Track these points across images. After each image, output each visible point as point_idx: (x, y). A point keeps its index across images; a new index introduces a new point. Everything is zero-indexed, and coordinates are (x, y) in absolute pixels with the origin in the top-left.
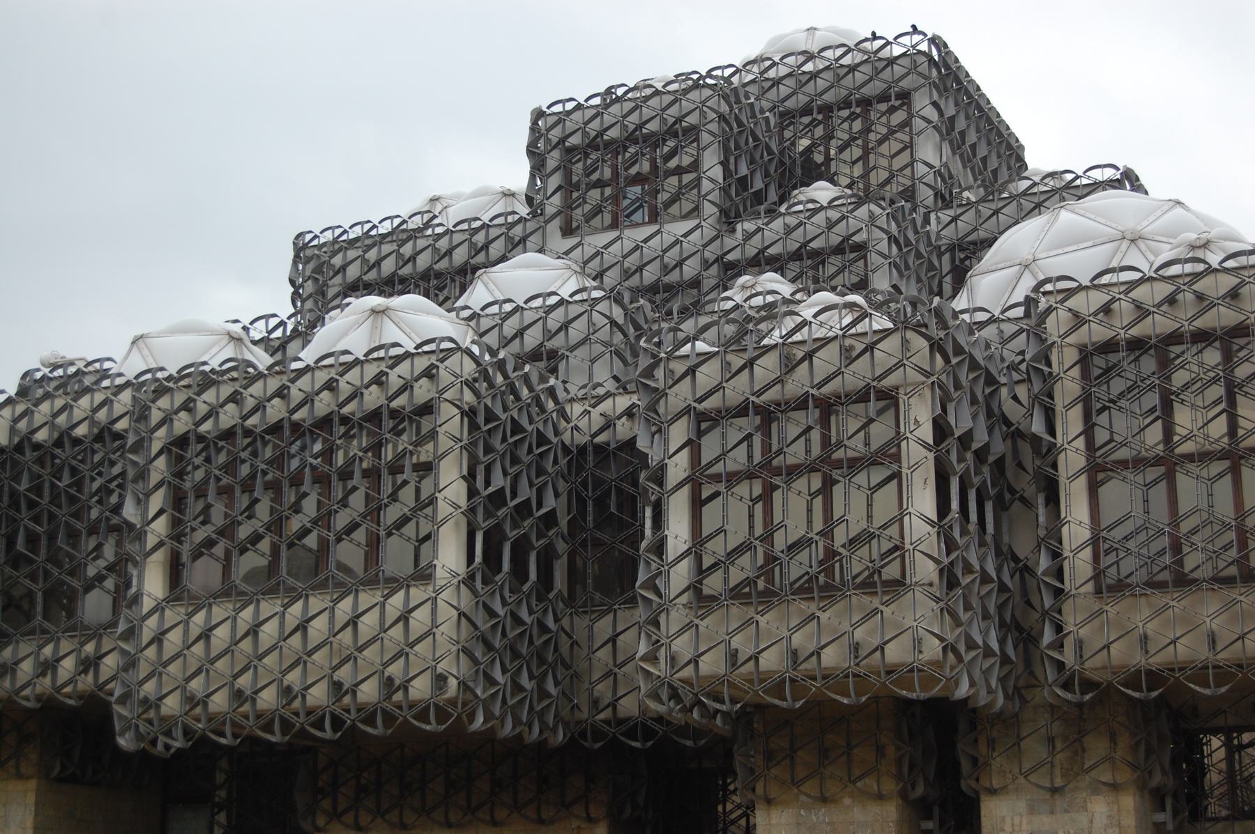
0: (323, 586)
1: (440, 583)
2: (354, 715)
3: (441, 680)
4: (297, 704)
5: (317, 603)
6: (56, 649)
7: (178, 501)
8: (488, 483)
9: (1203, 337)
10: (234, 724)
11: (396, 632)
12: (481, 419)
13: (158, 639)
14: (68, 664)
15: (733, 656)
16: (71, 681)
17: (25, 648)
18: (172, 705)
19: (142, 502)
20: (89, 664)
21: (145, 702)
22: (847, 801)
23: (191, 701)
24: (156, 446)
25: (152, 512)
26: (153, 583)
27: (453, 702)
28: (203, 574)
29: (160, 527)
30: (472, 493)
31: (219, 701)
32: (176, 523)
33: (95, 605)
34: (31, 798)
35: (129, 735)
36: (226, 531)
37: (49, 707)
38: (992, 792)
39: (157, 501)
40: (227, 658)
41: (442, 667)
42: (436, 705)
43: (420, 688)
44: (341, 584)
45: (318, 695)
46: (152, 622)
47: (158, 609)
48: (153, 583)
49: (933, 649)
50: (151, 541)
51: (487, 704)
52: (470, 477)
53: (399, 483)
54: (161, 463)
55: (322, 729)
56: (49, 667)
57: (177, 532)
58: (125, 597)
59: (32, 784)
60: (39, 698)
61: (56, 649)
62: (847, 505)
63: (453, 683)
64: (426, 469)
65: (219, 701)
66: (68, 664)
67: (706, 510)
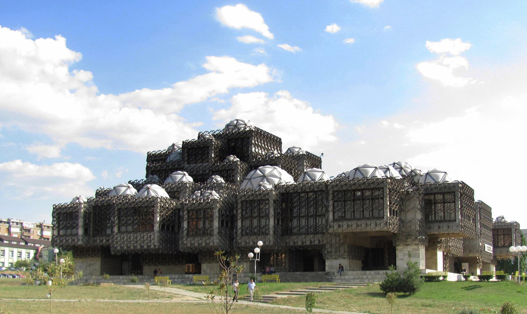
0: (146, 231)
1: (155, 232)
2: (143, 250)
3: (155, 246)
4: (143, 248)
5: (145, 234)
6: (103, 238)
7: (119, 219)
8: (277, 211)
9: (368, 189)
10: (148, 251)
11: (135, 240)
12: (276, 201)
13: (117, 238)
14: (105, 241)
15: (246, 243)
16: (105, 243)
17: (98, 238)
18: (119, 248)
19: (114, 217)
20: (108, 241)
21: (115, 248)
22: (213, 263)
23: (148, 246)
24: (116, 210)
25: (115, 220)
26: (116, 230)
27: (157, 249)
28: (123, 229)
29: (117, 222)
30: (275, 213)
31: (125, 248)
32: (119, 221)
33: (108, 231)
34: (100, 260)
35: (113, 252)
36: (126, 223)
37: (102, 247)
38: (398, 245)
39: (116, 218)
40: (139, 241)
41: (155, 244)
42: (302, 246)
43: (152, 247)
44: (135, 232)
45: (139, 247)
46: (116, 236)
47: (117, 234)
48: (116, 230)
49: (272, 243)
50: (185, 219)
51: (162, 249)
52: (274, 210)
53: (128, 219)
54: (116, 212)
55: (153, 251)
56: (102, 241)
57: (119, 223)
58: (112, 232)
59: (100, 258)
60: (100, 246)
61: (103, 238)
62: (319, 222)
63: (272, 242)
64: (383, 198)
65: (125, 248)
66: (105, 241)
67: (243, 222)
